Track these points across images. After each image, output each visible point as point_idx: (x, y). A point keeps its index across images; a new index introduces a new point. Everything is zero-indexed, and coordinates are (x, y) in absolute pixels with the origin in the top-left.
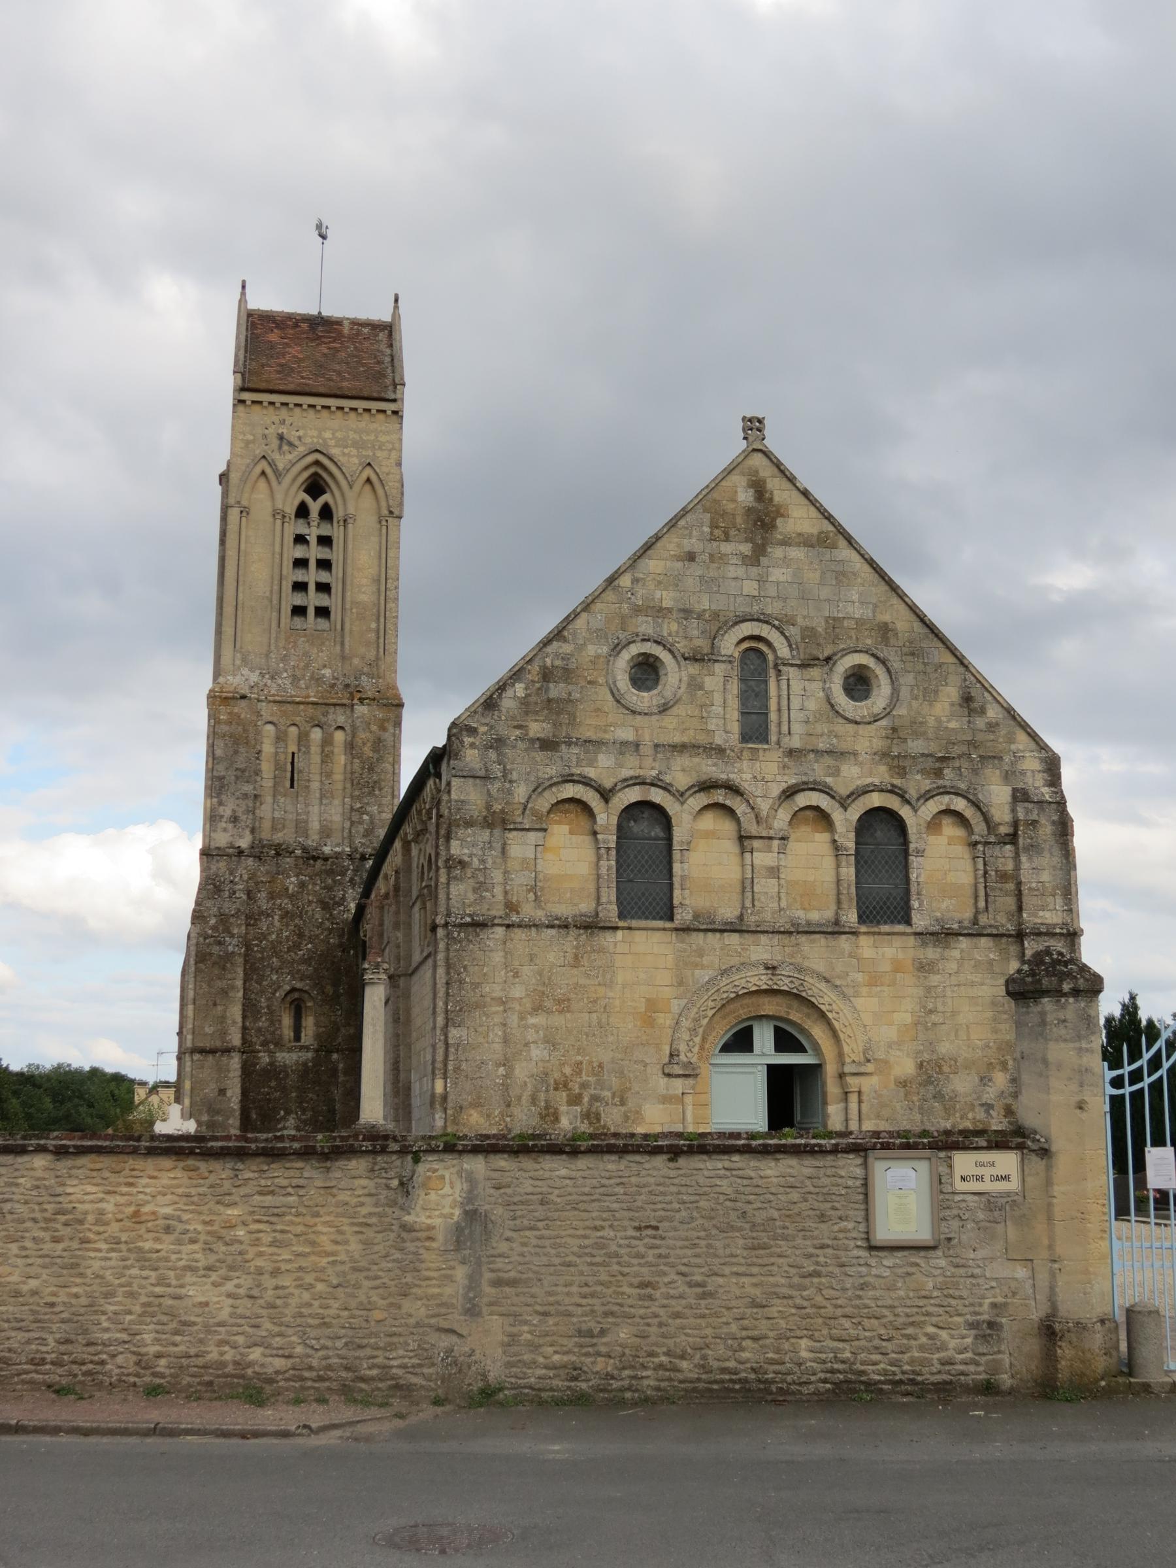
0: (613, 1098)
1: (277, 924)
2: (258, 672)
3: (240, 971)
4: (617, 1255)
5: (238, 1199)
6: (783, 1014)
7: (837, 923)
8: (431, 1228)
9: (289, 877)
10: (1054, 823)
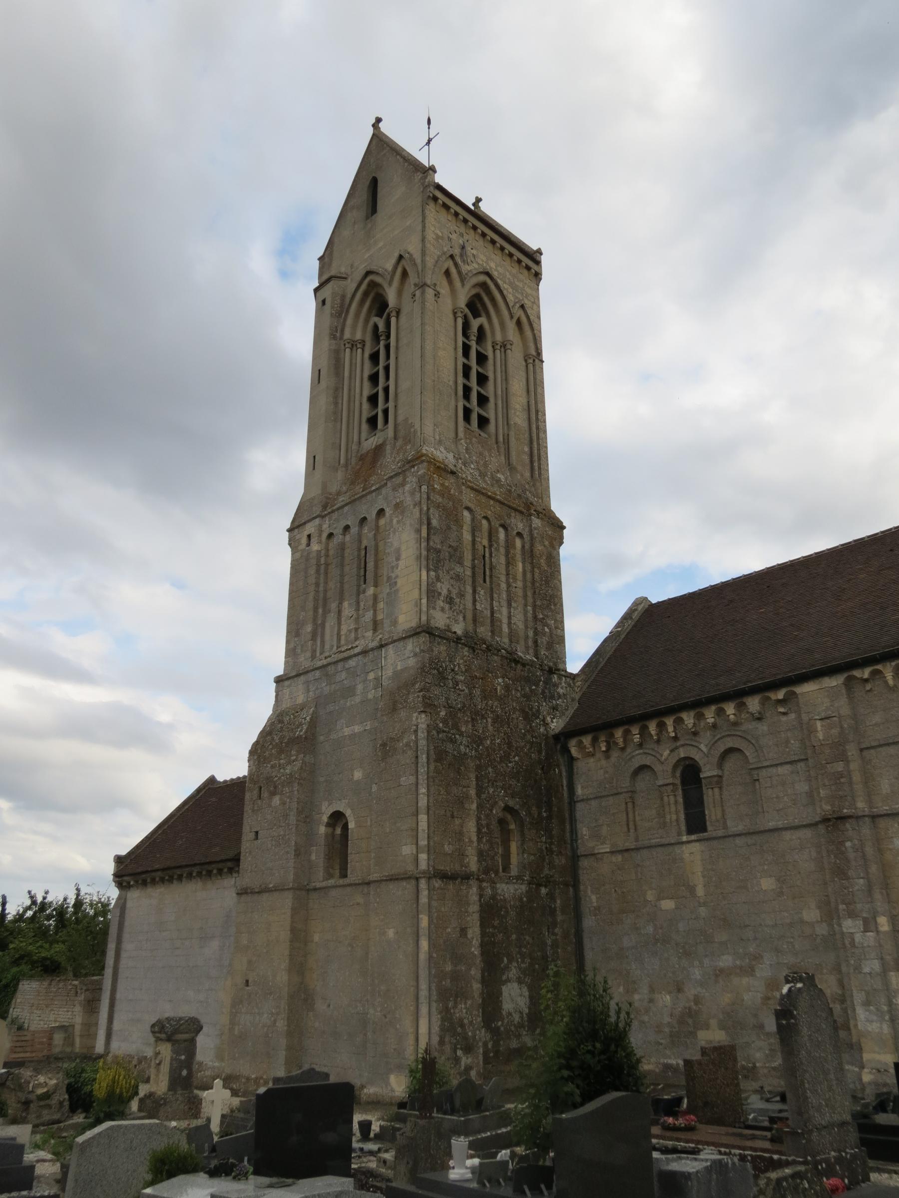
1: (490, 728)
9: (497, 678)
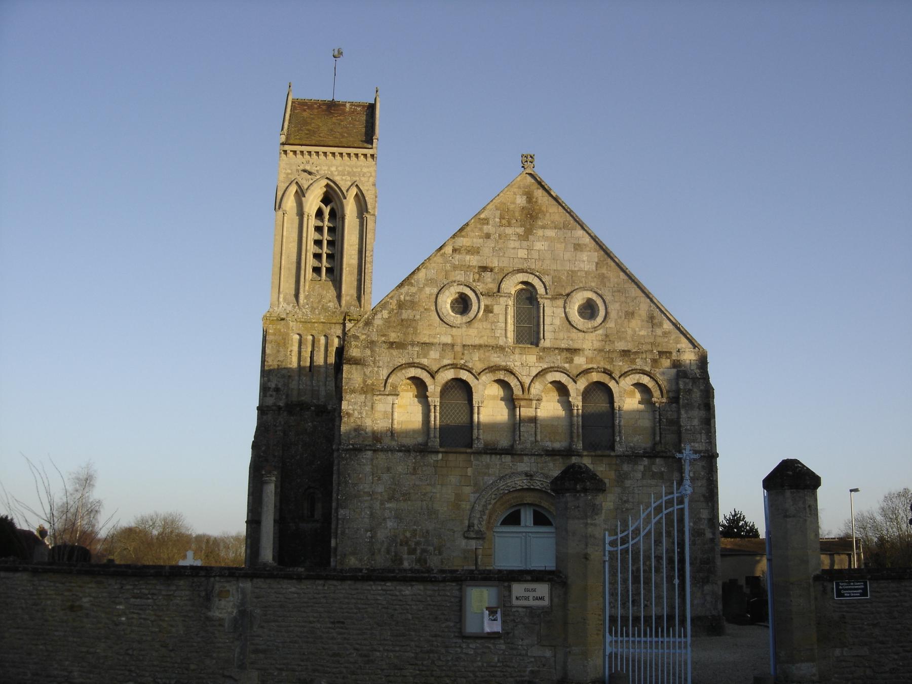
7: (426, 444)
8: (221, 619)
10: (701, 391)
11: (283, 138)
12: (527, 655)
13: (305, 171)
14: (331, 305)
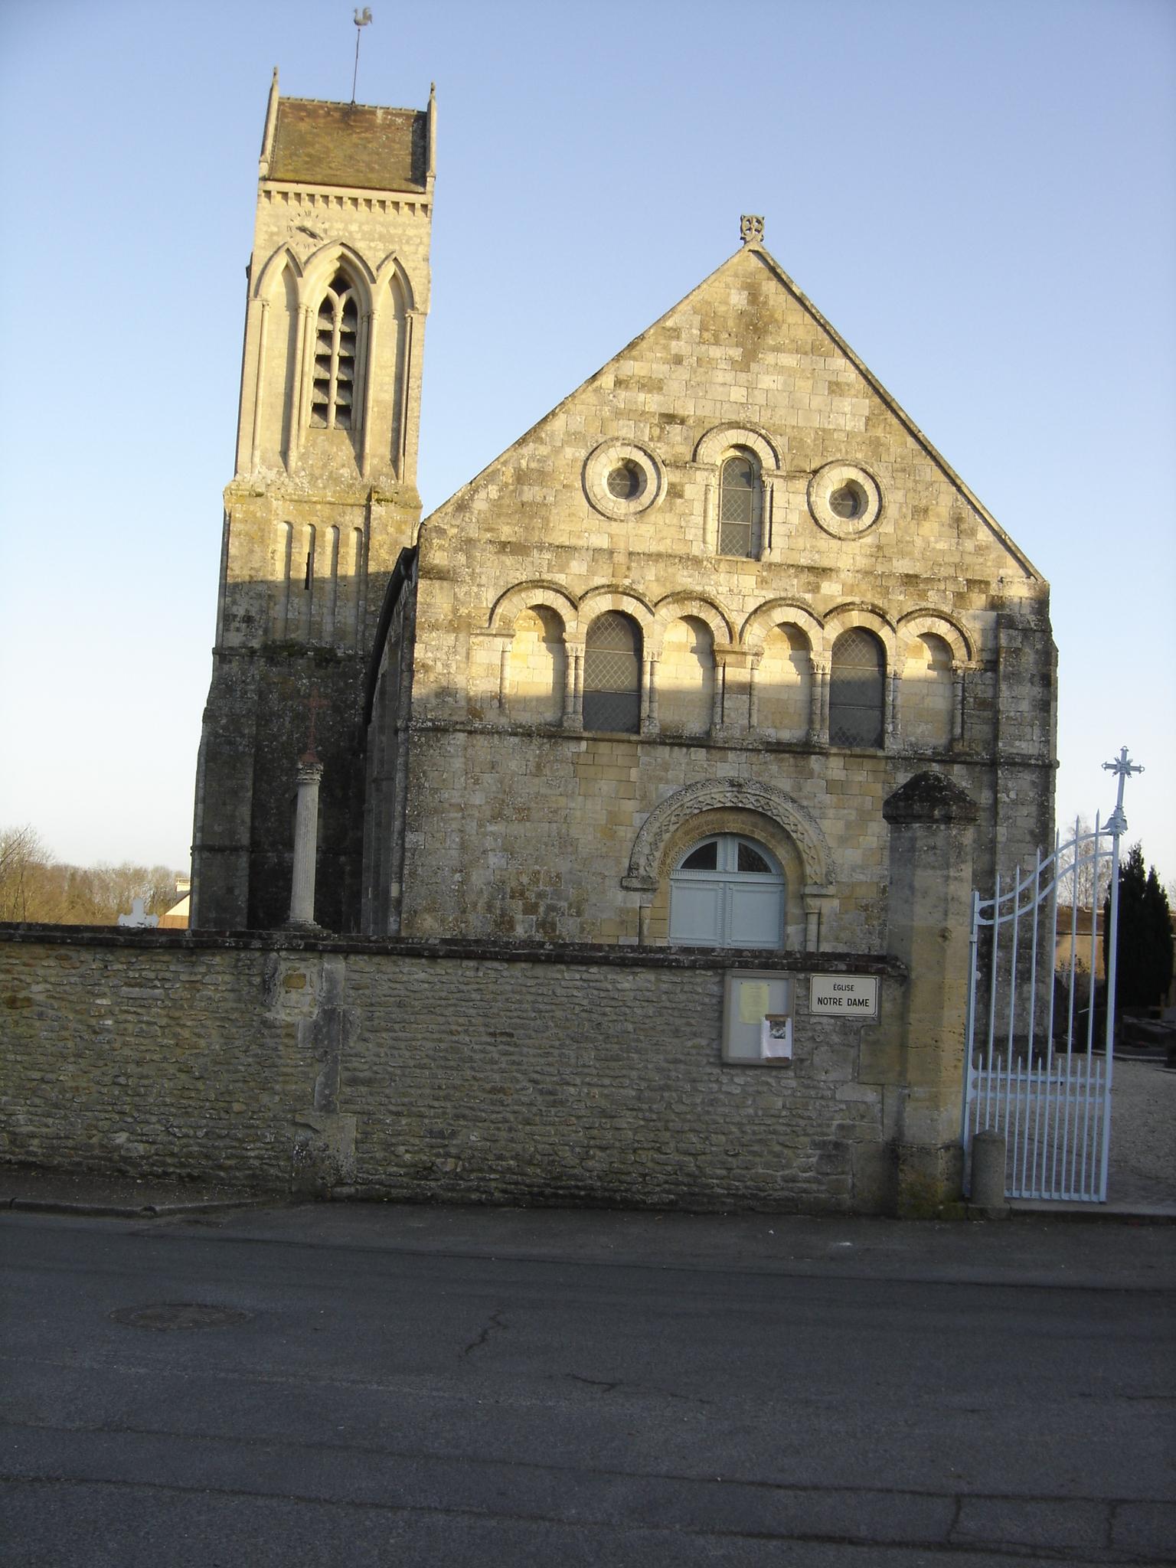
0: (569, 908)
2: (275, 470)
3: (250, 771)
4: (471, 1060)
5: (107, 990)
6: (747, 833)
7: (559, 724)
9: (301, 678)
10: (1037, 652)
11: (264, 169)
12: (833, 1098)
13: (303, 230)
14: (345, 472)
